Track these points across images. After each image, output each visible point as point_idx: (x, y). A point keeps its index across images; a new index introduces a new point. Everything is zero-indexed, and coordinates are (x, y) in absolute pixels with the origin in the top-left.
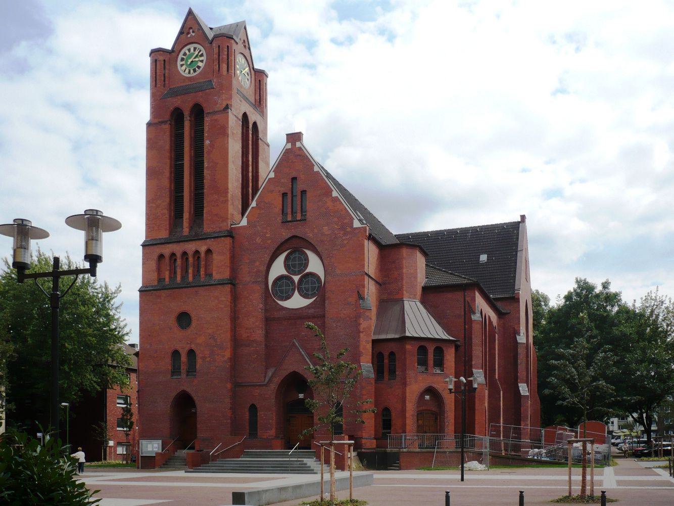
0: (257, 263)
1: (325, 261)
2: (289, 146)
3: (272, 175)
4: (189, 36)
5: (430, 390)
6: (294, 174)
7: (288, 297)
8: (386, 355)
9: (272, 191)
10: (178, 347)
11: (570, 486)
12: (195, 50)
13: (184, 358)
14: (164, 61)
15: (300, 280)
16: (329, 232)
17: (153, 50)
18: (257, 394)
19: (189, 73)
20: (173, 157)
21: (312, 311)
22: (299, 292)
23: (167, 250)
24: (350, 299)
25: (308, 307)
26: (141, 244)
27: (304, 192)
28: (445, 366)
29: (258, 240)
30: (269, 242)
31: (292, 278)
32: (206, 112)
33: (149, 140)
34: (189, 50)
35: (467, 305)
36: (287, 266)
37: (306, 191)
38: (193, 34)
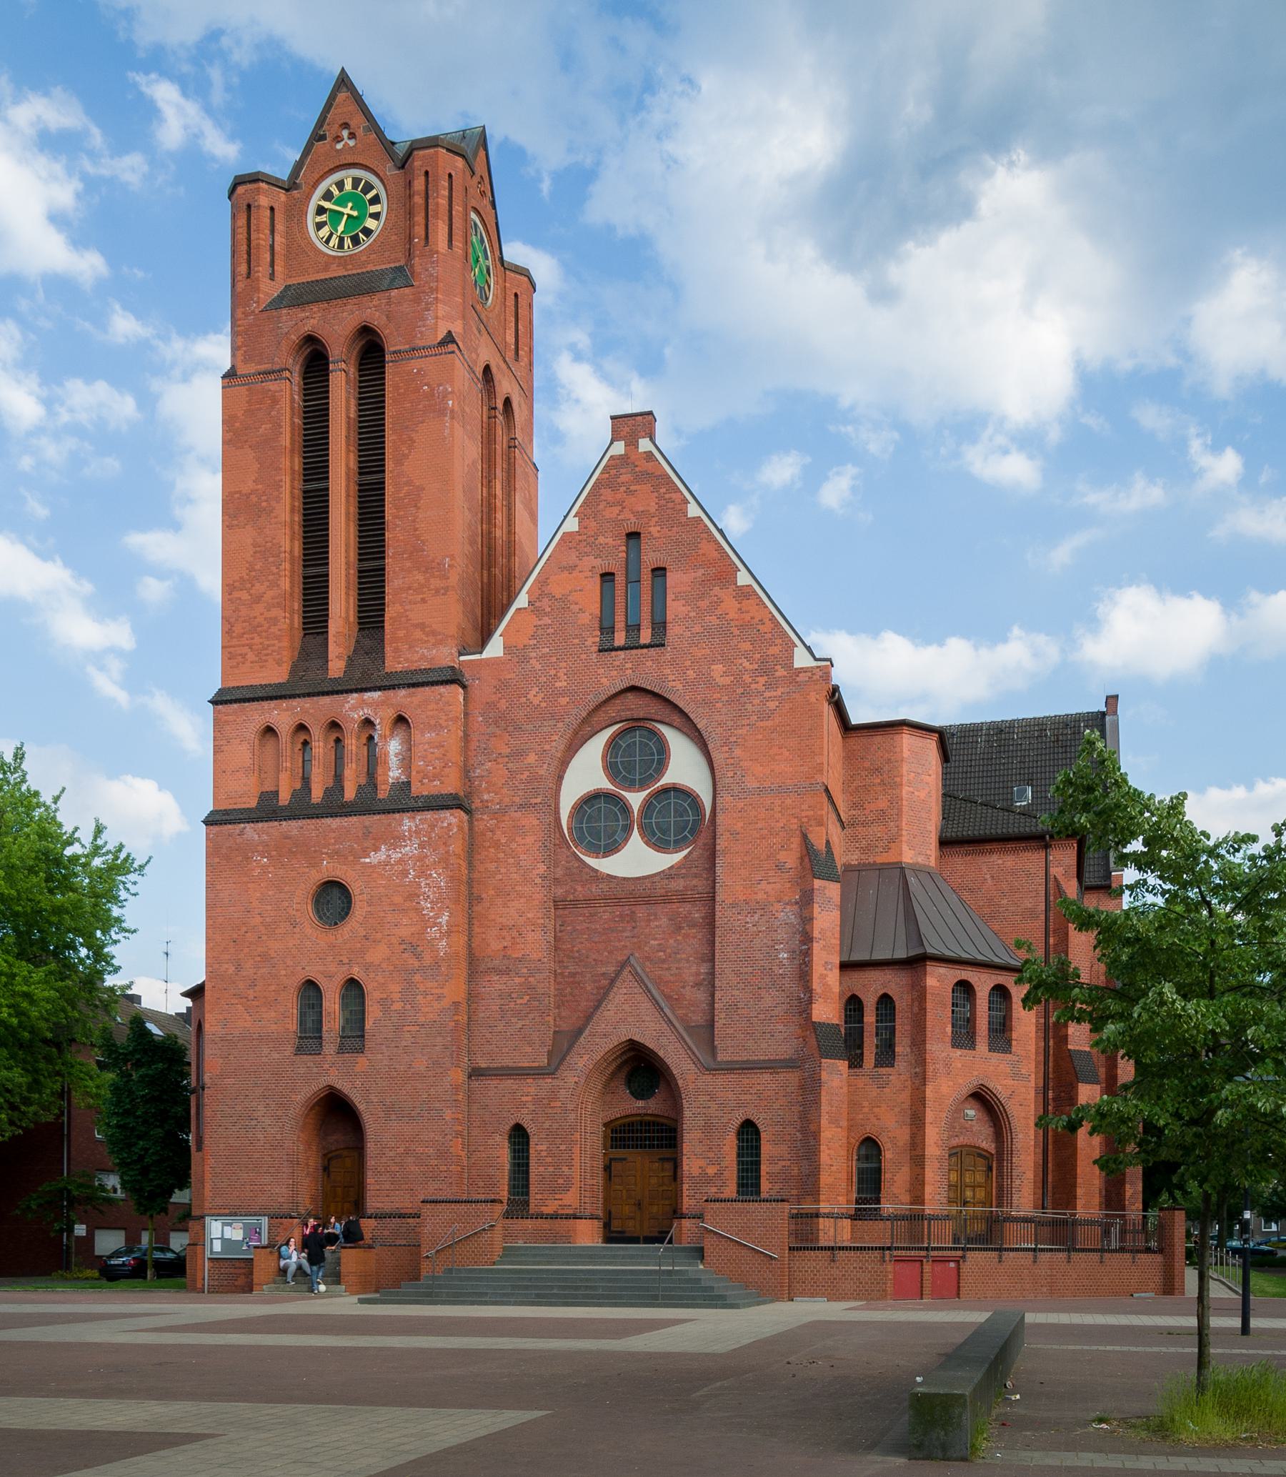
0: (532, 758)
1: (717, 756)
2: (619, 448)
3: (572, 525)
4: (339, 146)
5: (982, 1098)
6: (631, 525)
7: (611, 849)
8: (870, 1003)
9: (571, 568)
10: (313, 972)
11: (1202, 1319)
12: (355, 186)
13: (332, 1003)
14: (272, 209)
15: (647, 806)
16: (728, 680)
17: (239, 176)
18: (529, 1098)
19: (341, 245)
20: (297, 468)
21: (678, 885)
22: (643, 835)
23: (282, 716)
24: (782, 856)
25: (668, 874)
26: (210, 698)
27: (660, 572)
28: (1014, 1036)
29: (535, 696)
30: (563, 701)
31: (641, 789)
32: (392, 349)
33: (229, 421)
34: (340, 185)
35: (1051, 884)
36: (611, 769)
37: (664, 569)
38: (352, 143)
